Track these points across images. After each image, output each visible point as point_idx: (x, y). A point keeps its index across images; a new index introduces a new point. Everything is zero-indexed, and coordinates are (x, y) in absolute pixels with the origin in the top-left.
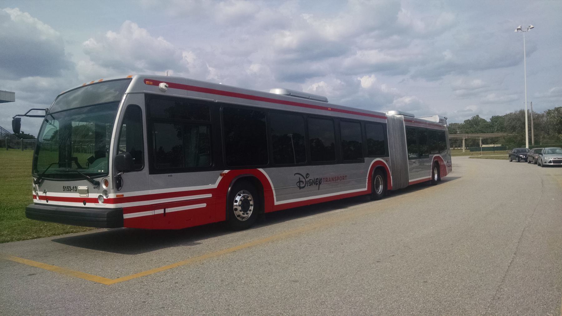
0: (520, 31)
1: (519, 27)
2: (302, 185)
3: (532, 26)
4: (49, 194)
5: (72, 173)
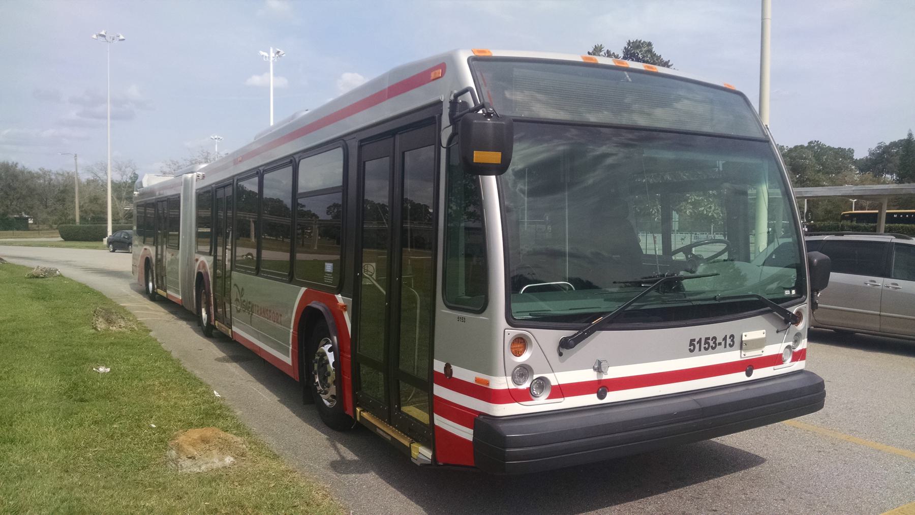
0: (102, 39)
1: (103, 33)
2: (694, 346)
3: (122, 37)
4: (614, 372)
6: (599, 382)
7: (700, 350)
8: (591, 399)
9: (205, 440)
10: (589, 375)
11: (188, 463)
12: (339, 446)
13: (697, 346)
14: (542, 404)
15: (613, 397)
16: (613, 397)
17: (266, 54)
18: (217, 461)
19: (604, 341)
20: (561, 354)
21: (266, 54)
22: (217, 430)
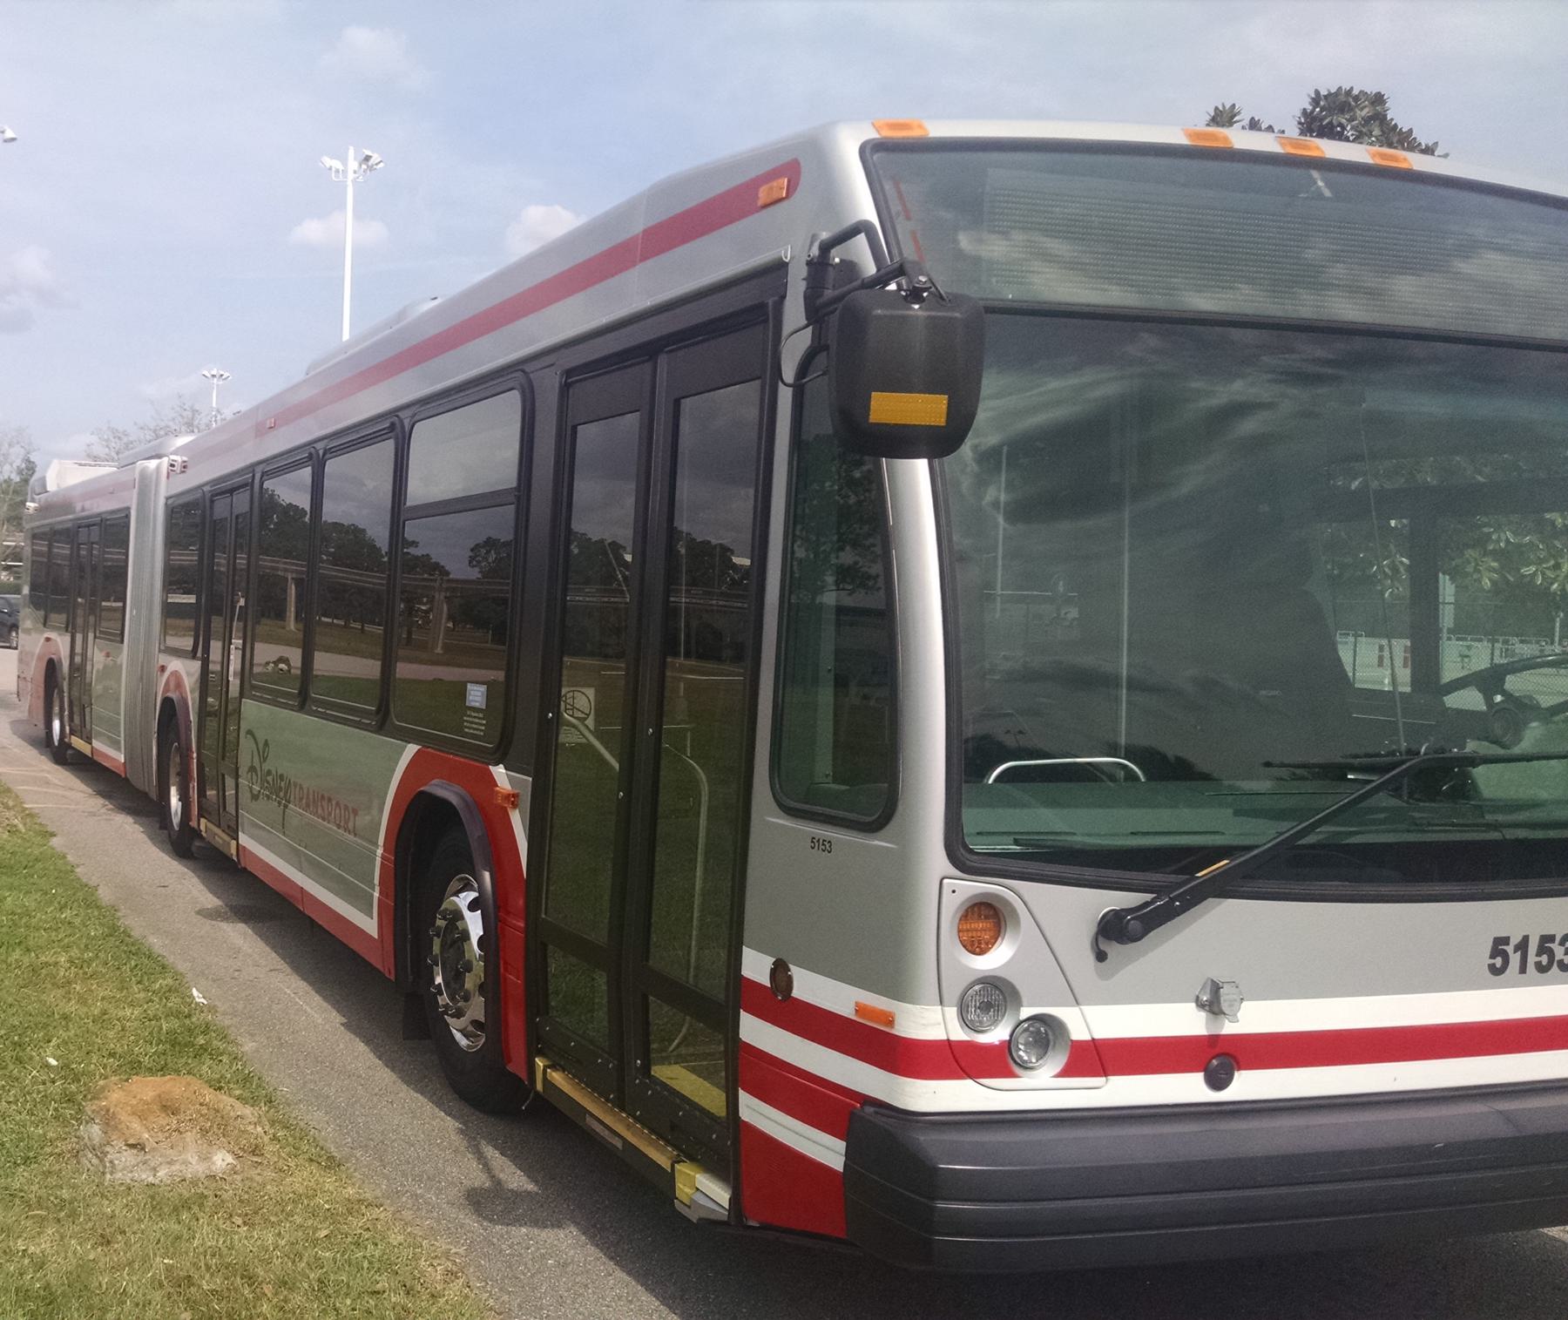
2: (1502, 959)
3: (9, 134)
4: (1255, 1017)
5: (1552, 834)
6: (1213, 1041)
7: (1523, 970)
8: (1188, 1088)
9: (169, 1108)
10: (1182, 1020)
11: (129, 1157)
12: (490, 1152)
13: (1515, 959)
14: (1041, 1088)
15: (1249, 1085)
16: (1249, 1085)
17: (336, 164)
18: (194, 1160)
19: (1228, 928)
20: (1101, 956)
21: (336, 164)
22: (197, 1084)
